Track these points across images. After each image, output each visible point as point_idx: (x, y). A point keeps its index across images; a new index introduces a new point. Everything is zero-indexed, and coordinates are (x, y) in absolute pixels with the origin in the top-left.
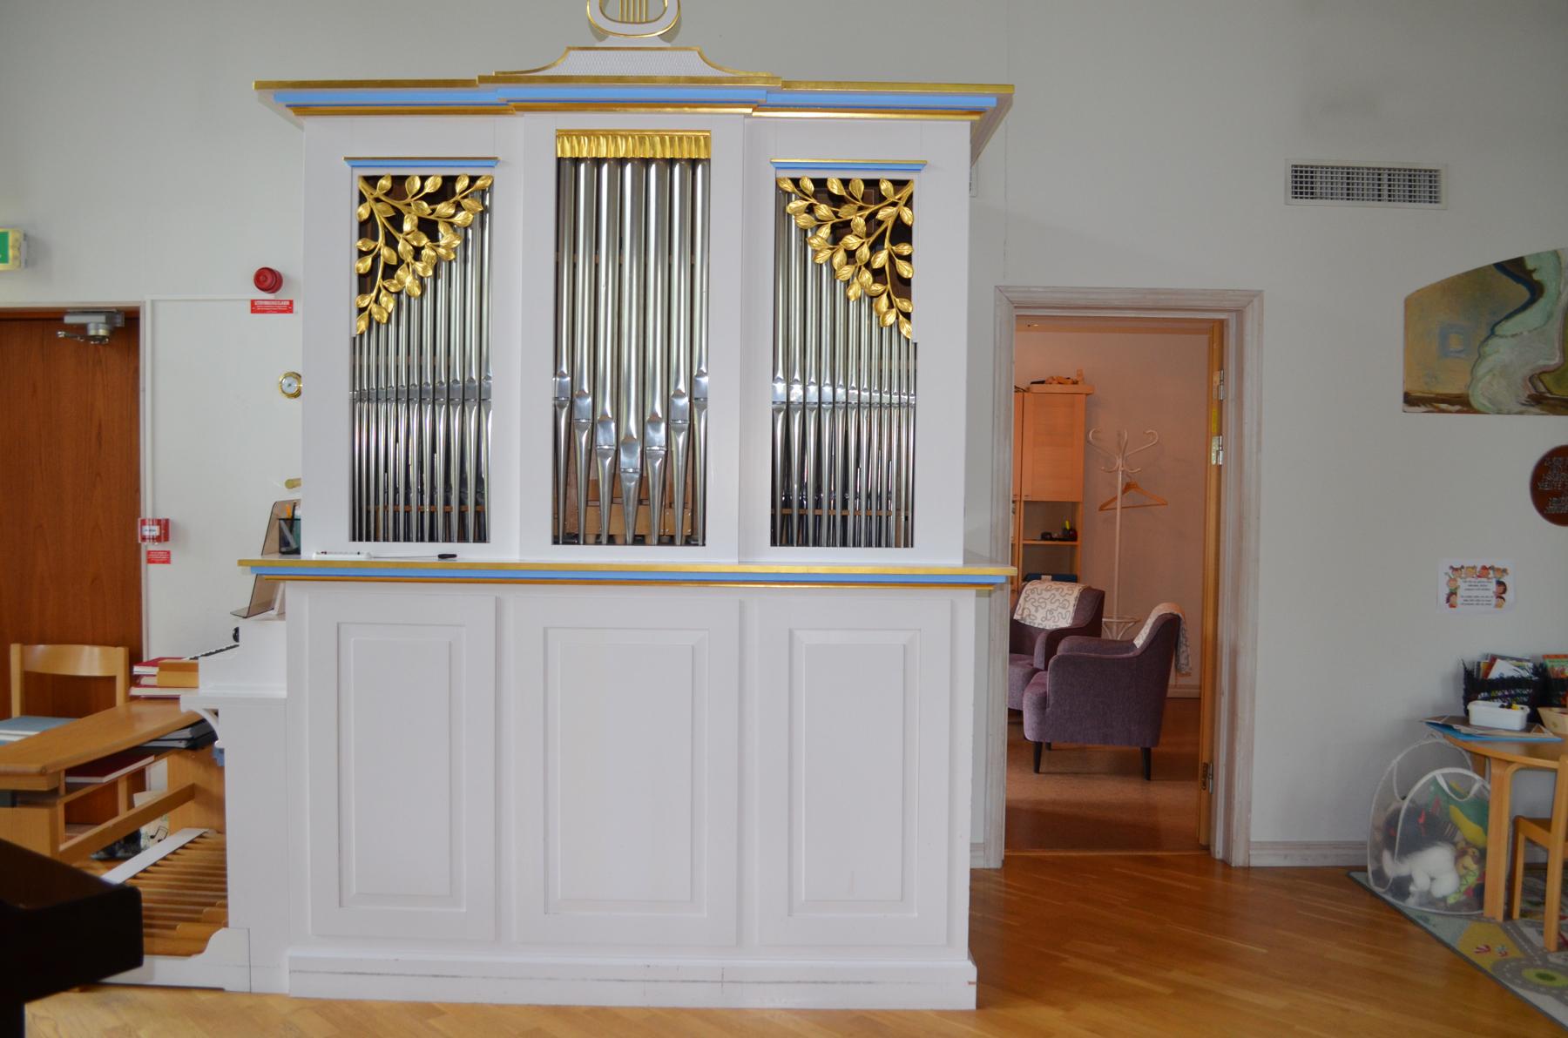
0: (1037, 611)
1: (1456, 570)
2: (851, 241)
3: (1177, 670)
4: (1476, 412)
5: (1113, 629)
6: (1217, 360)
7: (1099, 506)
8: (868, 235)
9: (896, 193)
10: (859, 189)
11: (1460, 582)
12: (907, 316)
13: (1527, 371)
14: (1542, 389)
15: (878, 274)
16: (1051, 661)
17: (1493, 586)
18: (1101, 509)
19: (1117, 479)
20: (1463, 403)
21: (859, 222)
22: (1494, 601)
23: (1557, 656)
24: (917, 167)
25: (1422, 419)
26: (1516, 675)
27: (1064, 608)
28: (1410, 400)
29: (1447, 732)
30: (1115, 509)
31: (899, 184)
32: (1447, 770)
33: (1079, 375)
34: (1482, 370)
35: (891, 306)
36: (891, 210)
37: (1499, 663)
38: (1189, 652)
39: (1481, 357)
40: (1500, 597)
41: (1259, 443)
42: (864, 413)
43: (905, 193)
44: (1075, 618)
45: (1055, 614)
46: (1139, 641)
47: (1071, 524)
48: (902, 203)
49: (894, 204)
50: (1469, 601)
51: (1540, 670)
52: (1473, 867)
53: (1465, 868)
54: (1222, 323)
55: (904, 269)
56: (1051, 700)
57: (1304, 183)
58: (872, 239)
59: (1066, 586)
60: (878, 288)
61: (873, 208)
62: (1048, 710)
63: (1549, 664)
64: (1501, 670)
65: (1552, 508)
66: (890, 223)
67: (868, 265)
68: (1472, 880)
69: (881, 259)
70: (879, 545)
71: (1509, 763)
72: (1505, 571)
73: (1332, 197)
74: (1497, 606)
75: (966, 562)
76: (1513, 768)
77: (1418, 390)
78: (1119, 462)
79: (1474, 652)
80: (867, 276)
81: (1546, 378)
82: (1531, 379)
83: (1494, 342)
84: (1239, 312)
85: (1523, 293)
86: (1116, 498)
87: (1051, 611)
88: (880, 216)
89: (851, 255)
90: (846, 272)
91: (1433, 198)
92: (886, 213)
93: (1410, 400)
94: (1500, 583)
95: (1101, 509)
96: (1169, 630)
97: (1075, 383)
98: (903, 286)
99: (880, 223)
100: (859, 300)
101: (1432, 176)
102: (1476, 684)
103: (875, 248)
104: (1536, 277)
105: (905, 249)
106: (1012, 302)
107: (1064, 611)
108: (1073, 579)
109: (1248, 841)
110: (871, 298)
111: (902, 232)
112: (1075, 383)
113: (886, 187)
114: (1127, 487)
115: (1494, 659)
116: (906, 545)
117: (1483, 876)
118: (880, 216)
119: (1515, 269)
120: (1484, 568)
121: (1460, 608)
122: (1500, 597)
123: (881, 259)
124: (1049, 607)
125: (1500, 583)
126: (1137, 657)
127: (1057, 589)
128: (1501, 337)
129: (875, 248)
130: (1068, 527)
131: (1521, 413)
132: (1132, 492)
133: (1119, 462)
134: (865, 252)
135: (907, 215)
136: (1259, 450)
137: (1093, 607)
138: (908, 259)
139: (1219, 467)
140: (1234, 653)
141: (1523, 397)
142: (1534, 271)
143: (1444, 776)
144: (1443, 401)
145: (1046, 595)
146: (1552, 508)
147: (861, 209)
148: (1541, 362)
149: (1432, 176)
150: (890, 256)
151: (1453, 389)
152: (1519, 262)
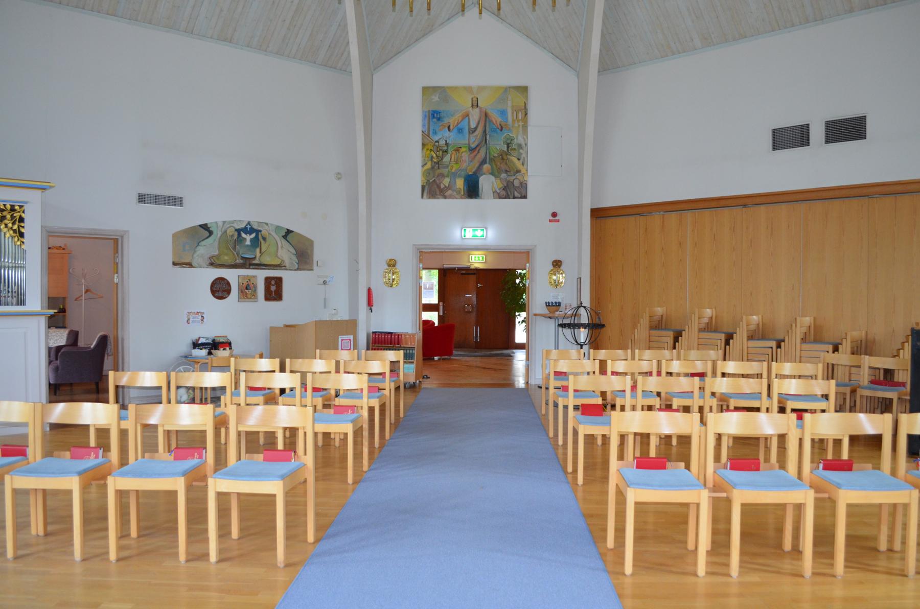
0: (50, 340)
1: (189, 313)
2: (6, 221)
3: (107, 354)
4: (194, 267)
5: (81, 343)
6: (116, 251)
7: (75, 298)
8: (11, 220)
9: (20, 209)
10: (8, 207)
11: (190, 316)
12: (23, 242)
13: (209, 256)
14: (213, 261)
15: (15, 231)
16: (60, 354)
17: (200, 317)
18: (76, 300)
19: (82, 288)
20: (190, 265)
21: (8, 217)
22: (201, 322)
23: (218, 337)
24: (26, 203)
25: (178, 269)
26: (206, 342)
27: (61, 338)
28: (174, 264)
29: (186, 358)
30: (82, 300)
31: (21, 207)
32: (183, 367)
33: (65, 246)
34: (195, 256)
35: (18, 240)
36: (19, 214)
37: (201, 339)
38: (110, 348)
39: (195, 252)
40: (202, 320)
41: (128, 276)
42: (10, 269)
43: (22, 209)
44: (67, 342)
45: (58, 341)
46: (92, 347)
47: (63, 306)
48: (22, 212)
49: (19, 212)
50: (194, 322)
51: (214, 340)
52: (192, 392)
53: (190, 393)
54: (117, 239)
55: (22, 230)
56: (60, 368)
57: (142, 199)
58: (13, 221)
59: (62, 330)
60: (15, 235)
61: (13, 213)
62: (59, 372)
63: (216, 339)
64: (202, 341)
65: (217, 295)
66: (18, 217)
67: (11, 228)
68: (191, 396)
69: (16, 227)
70: (21, 305)
71: (199, 362)
72: (203, 313)
73: (150, 203)
74: (202, 323)
75: (41, 309)
76: (200, 364)
77: (176, 261)
78: (83, 281)
79: (195, 337)
80: (11, 232)
81: (214, 258)
82: (210, 258)
83: (199, 248)
84: (122, 237)
85: (207, 234)
86: (82, 296)
87: (56, 340)
88: (15, 215)
89: (6, 225)
90: (5, 230)
91: (181, 205)
92: (17, 215)
93: (174, 264)
94: (202, 317)
95: (76, 300)
96: (104, 340)
97: (64, 249)
98: (22, 235)
99: (15, 217)
100: (9, 238)
101: (181, 199)
102: (196, 345)
103: (14, 223)
104: (211, 229)
105: (22, 224)
106: (48, 231)
107: (62, 340)
108: (64, 327)
109: (130, 397)
110: (12, 237)
111: (21, 220)
112: (64, 249)
113: (17, 208)
114: (87, 291)
115: (199, 338)
116: (24, 305)
117: (194, 395)
118: (15, 215)
119: (205, 227)
120: (197, 312)
121: (191, 324)
122: (202, 320)
123: (16, 227)
124: (56, 338)
125: (202, 317)
126: (92, 350)
127: (59, 331)
128: (201, 246)
129: (14, 223)
130: (62, 307)
131: (207, 268)
132: (88, 293)
133: (83, 281)
134: (10, 225)
135: (23, 215)
136: (128, 278)
137: (74, 337)
138: (23, 227)
139: (117, 283)
140: (123, 340)
141: (208, 263)
142: (210, 227)
143: (183, 368)
144: (184, 264)
145: (54, 334)
146: (217, 295)
147: (9, 213)
148: (213, 253)
149: (181, 199)
150: (18, 226)
151: (187, 261)
152: (206, 225)
